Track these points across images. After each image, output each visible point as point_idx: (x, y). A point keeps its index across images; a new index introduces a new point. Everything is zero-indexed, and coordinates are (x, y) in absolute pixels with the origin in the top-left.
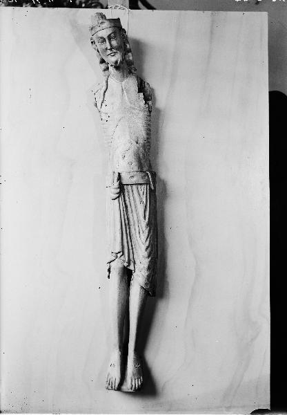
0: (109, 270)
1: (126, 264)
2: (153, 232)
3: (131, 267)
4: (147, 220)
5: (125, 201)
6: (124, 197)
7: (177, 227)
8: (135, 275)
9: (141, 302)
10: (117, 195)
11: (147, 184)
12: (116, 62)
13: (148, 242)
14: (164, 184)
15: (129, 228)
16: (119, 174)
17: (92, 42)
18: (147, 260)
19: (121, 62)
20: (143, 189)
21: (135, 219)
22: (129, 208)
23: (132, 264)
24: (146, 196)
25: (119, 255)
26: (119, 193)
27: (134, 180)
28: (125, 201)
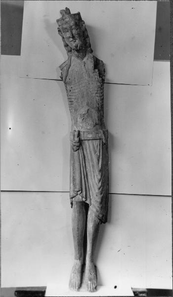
0: (72, 204)
1: (84, 199)
2: (102, 182)
3: (88, 202)
4: (100, 167)
5: (83, 152)
6: (83, 150)
7: (76, 273)
8: (91, 207)
9: (28, 290)
10: (78, 148)
11: (100, 139)
12: (76, 46)
13: (100, 183)
14: (112, 136)
15: (85, 162)
16: (79, 131)
17: (59, 31)
18: (100, 196)
19: (81, 46)
20: (97, 143)
21: (92, 185)
22: (86, 158)
23: (88, 200)
24: (100, 149)
25: (79, 193)
26: (78, 147)
27: (90, 136)
28: (83, 152)
